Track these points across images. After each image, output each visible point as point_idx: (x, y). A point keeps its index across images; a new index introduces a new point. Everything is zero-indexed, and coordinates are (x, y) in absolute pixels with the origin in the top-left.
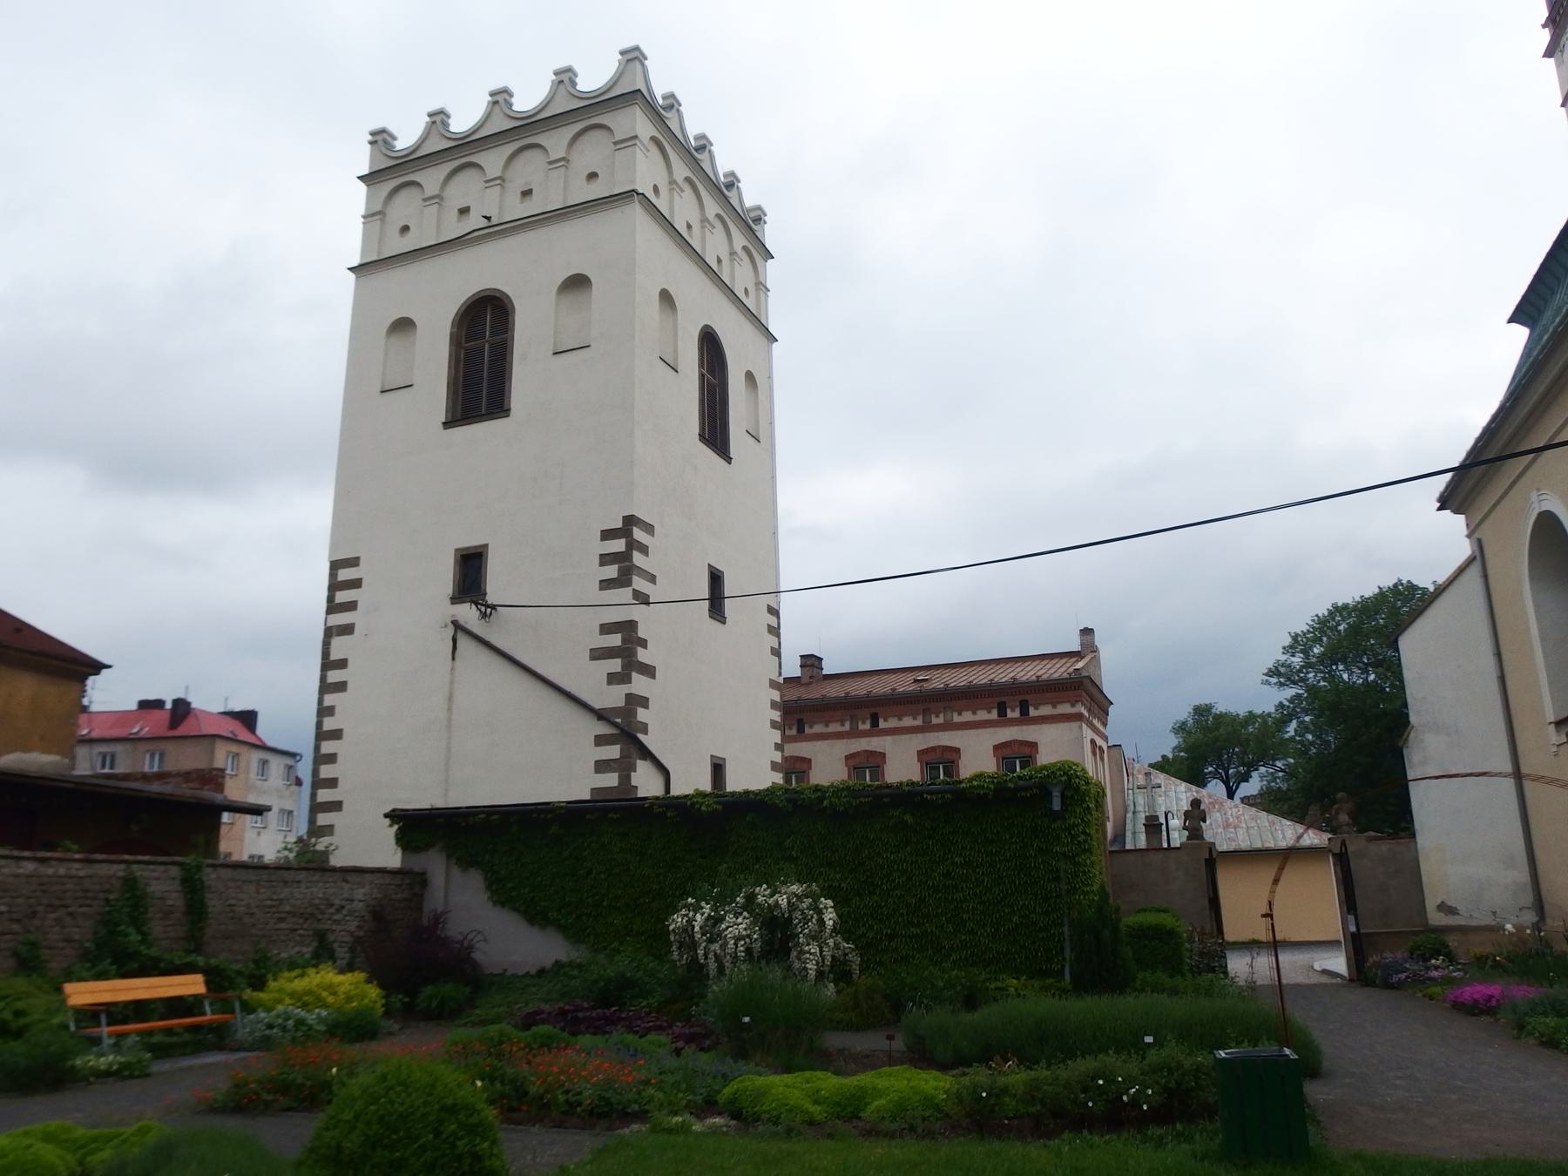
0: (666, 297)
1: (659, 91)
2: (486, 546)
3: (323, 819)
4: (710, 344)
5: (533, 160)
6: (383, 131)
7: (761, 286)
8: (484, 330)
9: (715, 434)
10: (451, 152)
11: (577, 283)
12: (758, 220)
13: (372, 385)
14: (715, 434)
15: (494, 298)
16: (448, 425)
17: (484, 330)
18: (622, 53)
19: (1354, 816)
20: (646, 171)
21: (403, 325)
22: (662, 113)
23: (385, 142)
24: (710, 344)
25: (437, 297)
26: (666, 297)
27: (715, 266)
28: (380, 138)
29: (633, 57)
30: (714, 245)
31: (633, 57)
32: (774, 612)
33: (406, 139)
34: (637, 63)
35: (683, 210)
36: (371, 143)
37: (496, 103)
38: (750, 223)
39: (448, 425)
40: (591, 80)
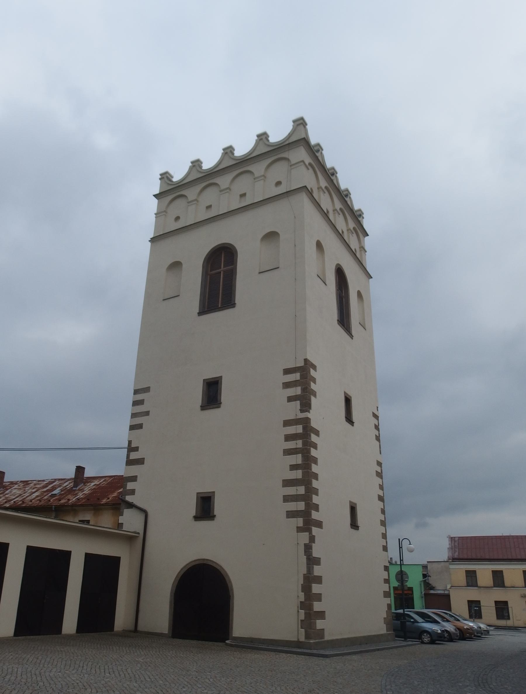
0: (319, 245)
1: (313, 141)
2: (221, 377)
3: (298, 474)
4: (340, 273)
5: (245, 180)
6: (167, 173)
7: (363, 249)
8: (221, 264)
9: (344, 320)
10: (201, 178)
11: (271, 236)
12: (360, 215)
13: (159, 296)
14: (344, 320)
15: (204, 565)
16: (200, 314)
17: (221, 264)
18: (294, 121)
19: (52, 507)
20: (306, 177)
21: (176, 265)
22: (315, 151)
23: (167, 178)
24: (340, 273)
25: (194, 251)
26: (319, 245)
27: (341, 233)
28: (165, 177)
29: (300, 123)
30: (340, 223)
31: (300, 123)
32: (376, 416)
33: (178, 176)
34: (302, 126)
35: (325, 202)
36: (160, 179)
37: (226, 153)
38: (357, 217)
39: (200, 314)
40: (277, 136)
